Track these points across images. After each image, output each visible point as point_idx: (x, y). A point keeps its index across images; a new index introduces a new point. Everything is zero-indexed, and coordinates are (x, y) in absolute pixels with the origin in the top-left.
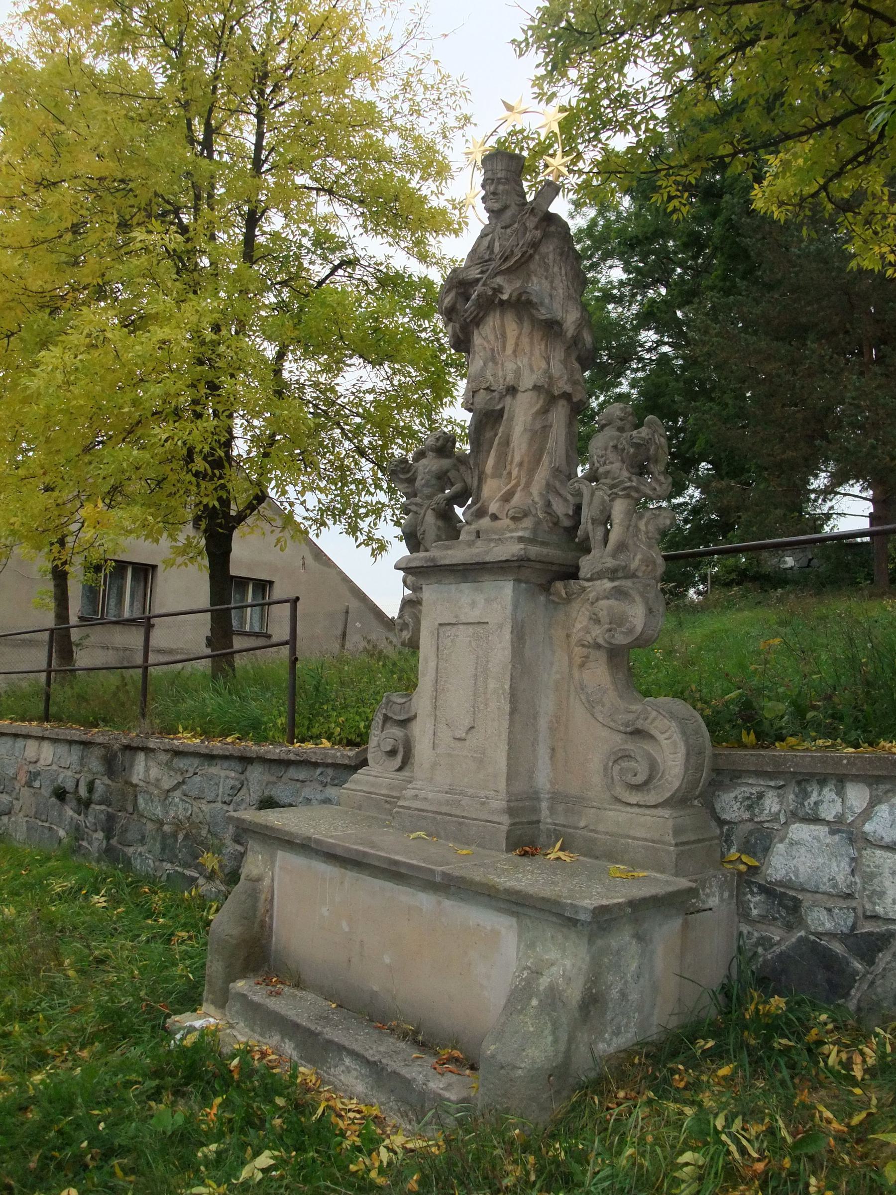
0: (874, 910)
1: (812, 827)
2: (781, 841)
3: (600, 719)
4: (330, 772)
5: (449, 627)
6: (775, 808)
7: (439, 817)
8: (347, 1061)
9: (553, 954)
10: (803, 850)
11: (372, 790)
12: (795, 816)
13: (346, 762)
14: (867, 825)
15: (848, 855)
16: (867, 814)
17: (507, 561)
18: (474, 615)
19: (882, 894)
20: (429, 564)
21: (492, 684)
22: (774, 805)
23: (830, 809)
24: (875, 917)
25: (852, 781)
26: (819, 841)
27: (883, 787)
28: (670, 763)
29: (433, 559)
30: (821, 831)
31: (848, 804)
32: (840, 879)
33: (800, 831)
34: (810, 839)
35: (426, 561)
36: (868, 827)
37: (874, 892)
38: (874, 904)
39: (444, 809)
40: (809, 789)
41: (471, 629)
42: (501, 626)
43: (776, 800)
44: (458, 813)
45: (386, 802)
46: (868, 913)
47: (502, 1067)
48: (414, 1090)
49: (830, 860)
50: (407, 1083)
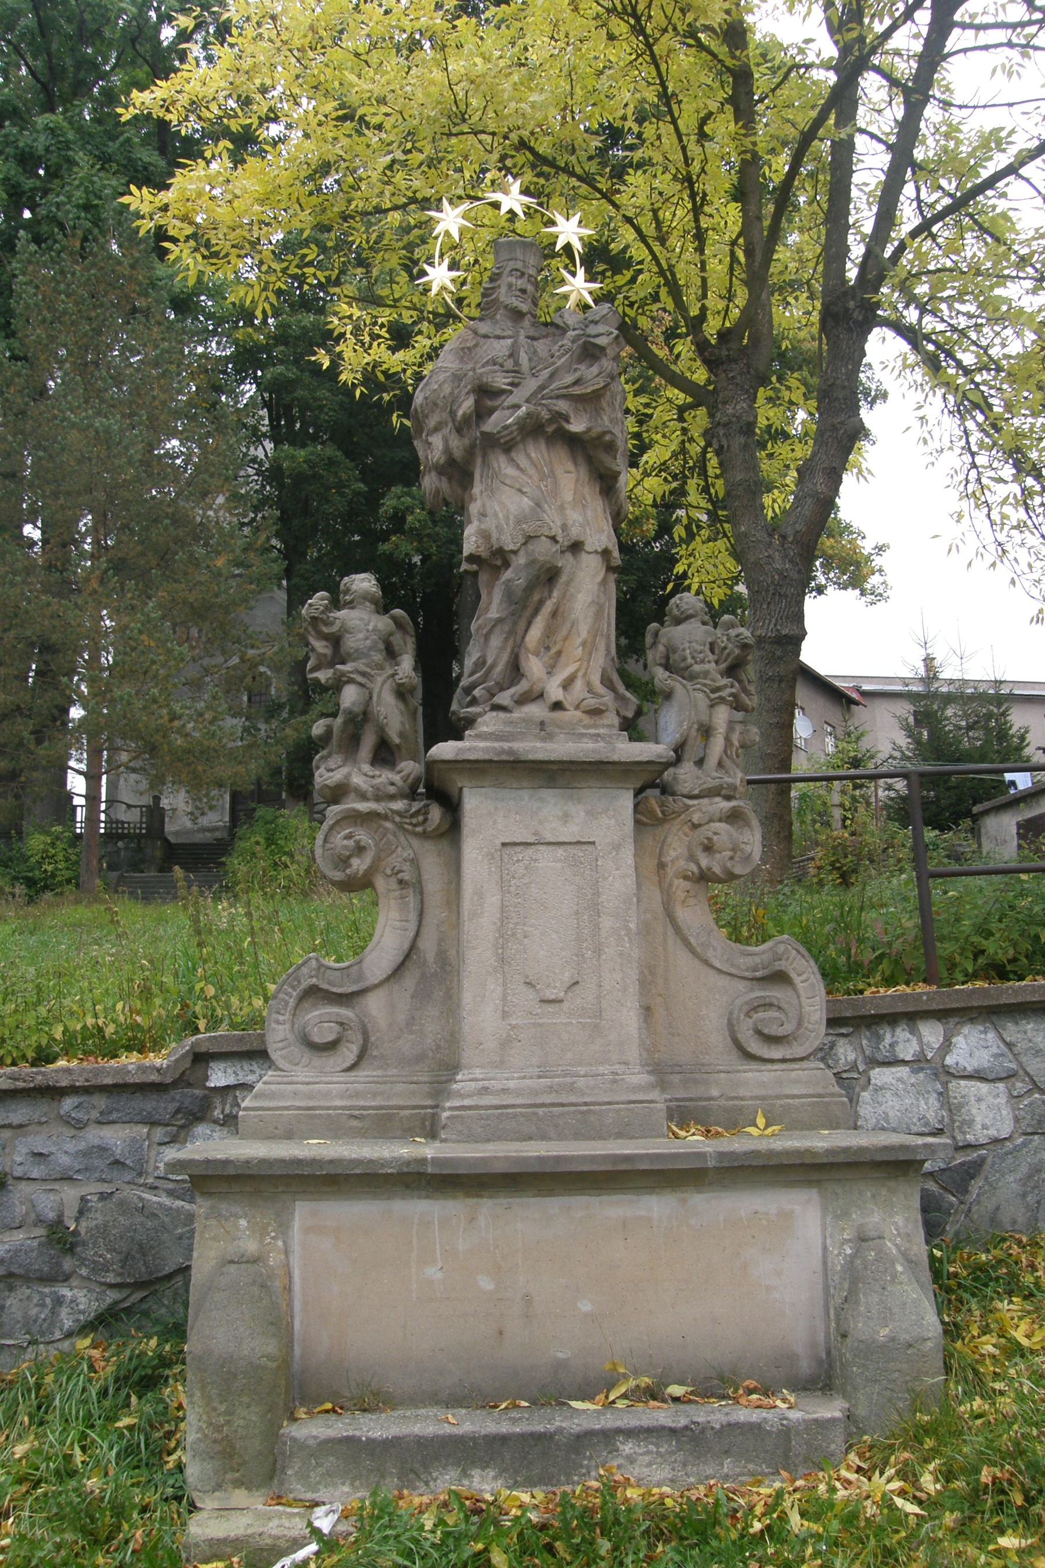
0: (965, 1140)
1: (893, 1070)
2: (864, 1089)
3: (718, 965)
4: (101, 1102)
5: (518, 849)
6: (851, 1057)
7: (541, 1111)
8: (627, 1448)
9: (875, 1218)
10: (888, 1094)
11: (311, 1104)
12: (874, 1062)
13: (154, 1078)
14: (947, 1058)
15: (935, 1091)
16: (947, 1046)
17: (648, 762)
18: (570, 832)
19: (970, 1123)
20: (504, 757)
21: (607, 923)
22: (849, 1053)
23: (908, 1049)
24: (969, 1147)
25: (921, 1018)
26: (903, 1083)
27: (952, 1021)
28: (808, 1009)
29: (511, 752)
30: (903, 1071)
31: (925, 1040)
32: (931, 1116)
33: (881, 1076)
34: (894, 1082)
35: (499, 754)
36: (949, 1060)
37: (963, 1122)
38: (964, 1133)
39: (548, 1099)
40: (881, 1032)
41: (560, 852)
42: (617, 847)
43: (849, 1048)
44: (573, 1099)
45: (355, 1117)
46: (961, 1144)
47: (910, 1346)
48: (769, 1432)
49: (917, 1099)
50: (755, 1429)
